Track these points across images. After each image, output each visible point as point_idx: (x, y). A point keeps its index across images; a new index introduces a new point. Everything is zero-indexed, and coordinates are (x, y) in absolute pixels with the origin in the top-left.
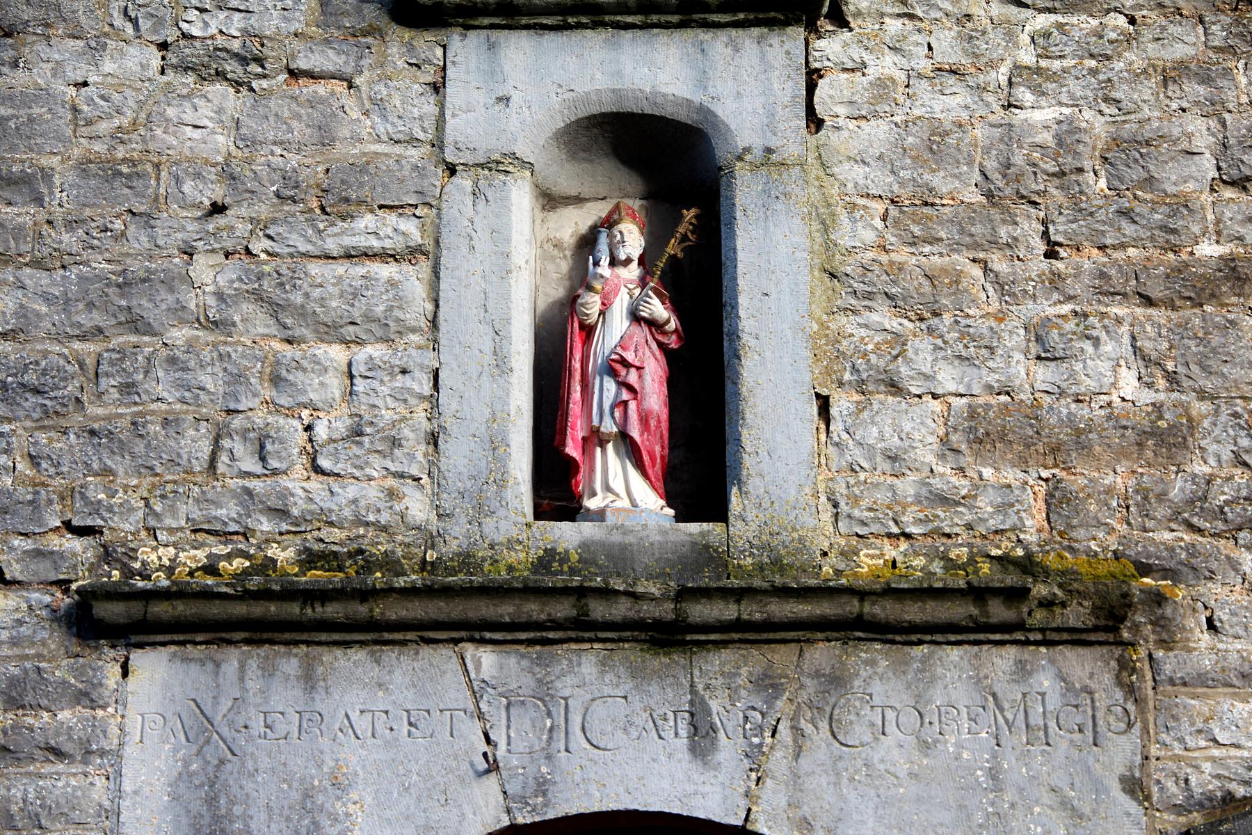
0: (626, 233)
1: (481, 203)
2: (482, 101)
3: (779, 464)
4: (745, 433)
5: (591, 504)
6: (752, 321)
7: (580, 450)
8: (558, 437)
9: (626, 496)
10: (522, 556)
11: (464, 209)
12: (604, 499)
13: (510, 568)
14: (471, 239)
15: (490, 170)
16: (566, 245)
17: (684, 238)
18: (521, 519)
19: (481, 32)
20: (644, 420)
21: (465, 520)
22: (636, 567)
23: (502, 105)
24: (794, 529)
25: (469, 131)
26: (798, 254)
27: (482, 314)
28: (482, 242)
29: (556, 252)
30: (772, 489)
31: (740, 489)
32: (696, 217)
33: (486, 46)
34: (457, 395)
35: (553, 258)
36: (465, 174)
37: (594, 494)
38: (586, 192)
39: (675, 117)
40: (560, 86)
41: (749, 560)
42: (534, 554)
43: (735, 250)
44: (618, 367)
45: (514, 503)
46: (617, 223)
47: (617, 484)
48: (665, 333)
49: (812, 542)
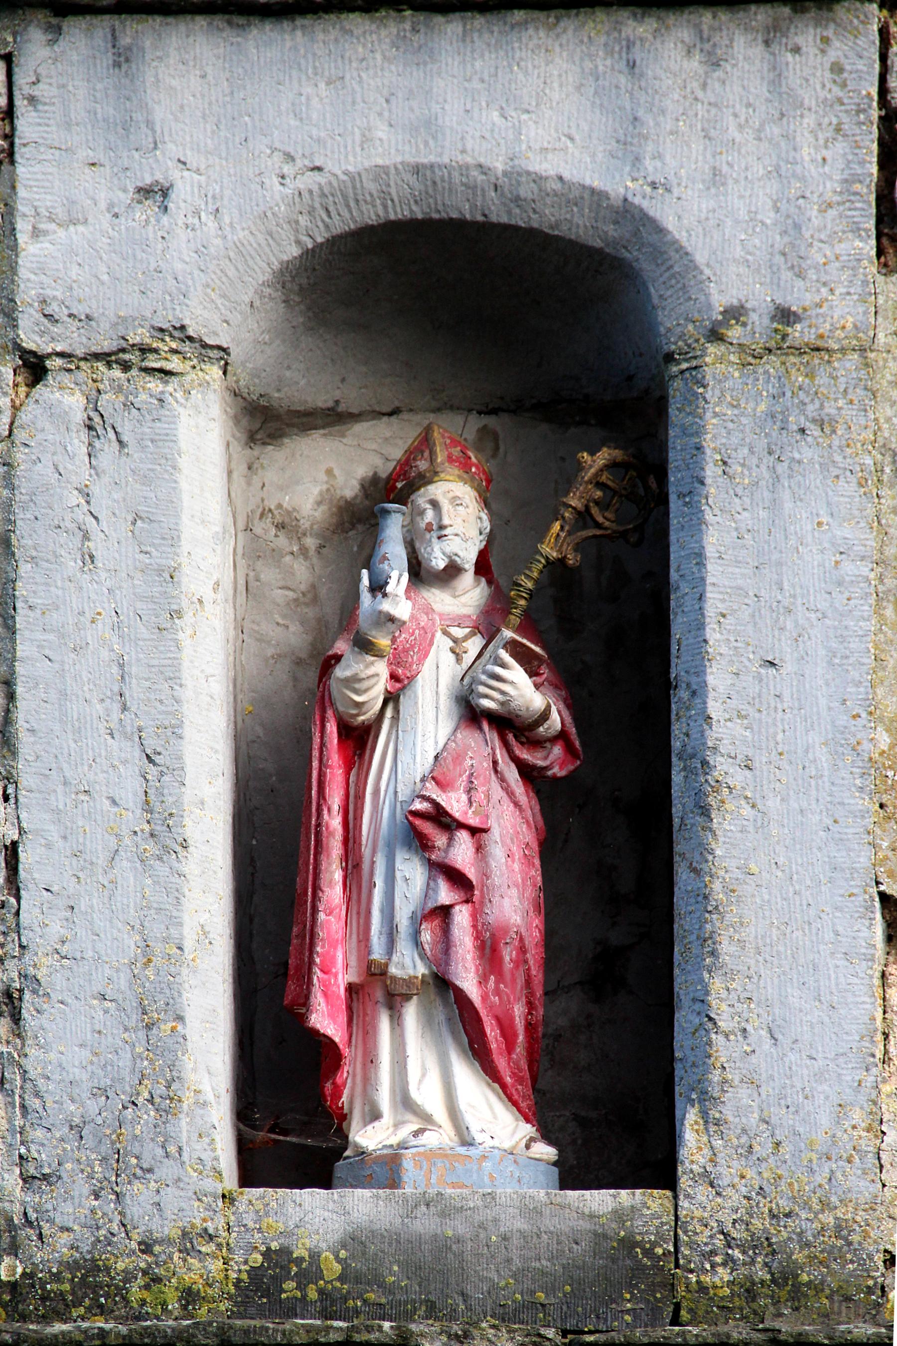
0: (446, 506)
1: (107, 448)
2: (103, 196)
3: (792, 1057)
4: (717, 984)
5: (368, 1137)
6: (737, 728)
7: (343, 1018)
8: (291, 986)
9: (446, 1123)
10: (215, 1266)
11: (66, 465)
12: (397, 1125)
13: (189, 1296)
14: (86, 537)
15: (126, 367)
16: (305, 524)
17: (583, 517)
18: (210, 1185)
19: (96, 20)
20: (489, 949)
21: (86, 1190)
22: (469, 1289)
23: (151, 207)
24: (825, 1205)
25: (74, 271)
26: (849, 568)
27: (116, 715)
28: (112, 543)
29: (282, 541)
30: (777, 1114)
31: (704, 1114)
32: (612, 466)
33: (109, 58)
34: (62, 903)
35: (276, 555)
36: (66, 378)
37: (375, 1115)
38: (352, 397)
39: (563, 231)
40: (290, 158)
41: (724, 1274)
42: (245, 1261)
43: (699, 557)
44: (428, 828)
45: (195, 1149)
46: (424, 480)
47: (427, 1093)
48: (536, 744)
49: (866, 1235)
